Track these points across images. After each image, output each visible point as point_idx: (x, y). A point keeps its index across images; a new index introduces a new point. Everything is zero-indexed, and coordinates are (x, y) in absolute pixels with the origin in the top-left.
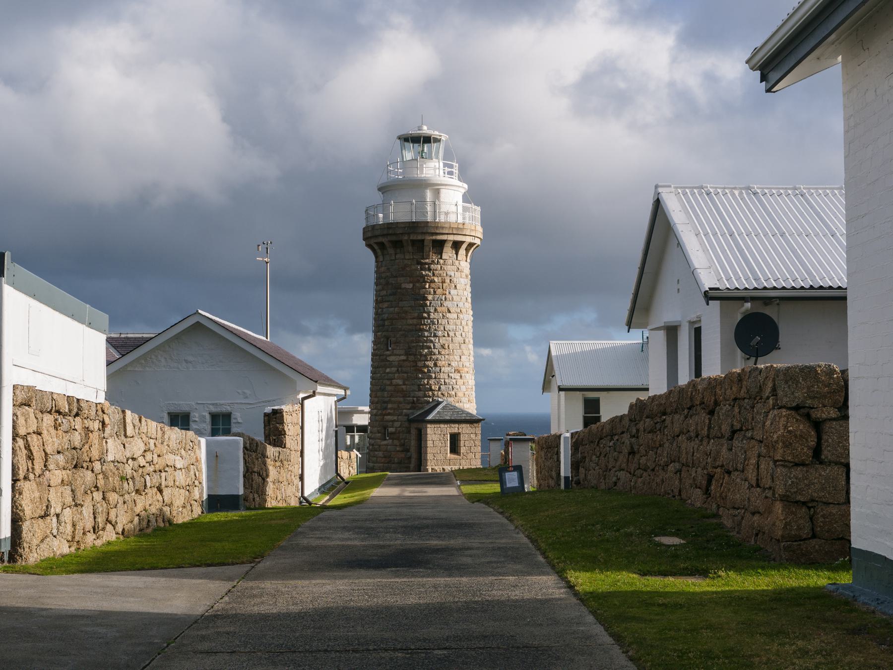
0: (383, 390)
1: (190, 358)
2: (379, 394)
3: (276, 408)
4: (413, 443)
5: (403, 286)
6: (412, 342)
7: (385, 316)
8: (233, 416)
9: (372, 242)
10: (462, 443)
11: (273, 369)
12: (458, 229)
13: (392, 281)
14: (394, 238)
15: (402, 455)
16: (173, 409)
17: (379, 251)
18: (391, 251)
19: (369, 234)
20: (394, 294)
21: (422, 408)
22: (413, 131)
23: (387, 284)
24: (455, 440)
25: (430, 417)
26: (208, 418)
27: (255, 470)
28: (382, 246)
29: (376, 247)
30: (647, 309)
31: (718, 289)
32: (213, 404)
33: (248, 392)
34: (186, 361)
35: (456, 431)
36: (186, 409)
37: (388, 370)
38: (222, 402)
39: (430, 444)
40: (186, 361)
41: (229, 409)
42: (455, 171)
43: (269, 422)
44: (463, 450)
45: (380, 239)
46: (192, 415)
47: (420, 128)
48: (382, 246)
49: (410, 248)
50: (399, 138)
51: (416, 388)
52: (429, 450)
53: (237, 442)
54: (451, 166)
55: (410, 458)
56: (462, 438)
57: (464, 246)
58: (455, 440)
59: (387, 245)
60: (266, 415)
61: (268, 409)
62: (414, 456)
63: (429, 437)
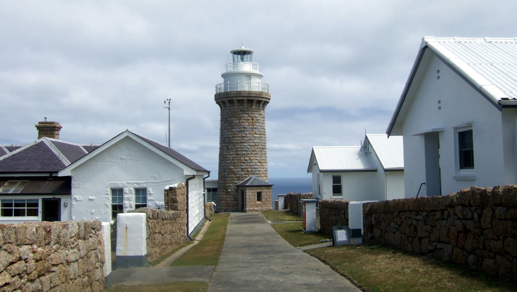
0: (225, 172)
1: (123, 157)
2: (223, 173)
3: (172, 186)
4: (240, 197)
5: (234, 121)
6: (238, 148)
7: (226, 136)
8: (148, 190)
9: (219, 101)
10: (263, 197)
11: (170, 163)
12: (259, 94)
13: (228, 119)
14: (229, 99)
15: (235, 202)
16: (114, 186)
17: (222, 106)
18: (228, 105)
19: (218, 97)
20: (230, 126)
21: (243, 180)
22: (239, 49)
23: (226, 121)
24: (259, 197)
25: (247, 184)
26: (134, 191)
27: (157, 231)
28: (224, 102)
29: (221, 103)
30: (402, 125)
31: (507, 99)
32: (136, 183)
33: (156, 176)
34: (121, 159)
35: (259, 191)
36: (120, 186)
37: (227, 162)
38: (141, 182)
39: (247, 197)
40: (121, 159)
41: (145, 185)
42: (258, 67)
43: (168, 194)
44: (263, 200)
45: (223, 100)
46: (124, 189)
47: (240, 47)
48: (224, 102)
49: (237, 104)
50: (231, 52)
51: (240, 170)
52: (247, 200)
53: (141, 217)
54: (256, 65)
55: (238, 204)
56: (263, 194)
57: (262, 103)
58: (259, 197)
59: (227, 102)
60: (165, 190)
61: (167, 188)
62: (240, 203)
63: (247, 194)
